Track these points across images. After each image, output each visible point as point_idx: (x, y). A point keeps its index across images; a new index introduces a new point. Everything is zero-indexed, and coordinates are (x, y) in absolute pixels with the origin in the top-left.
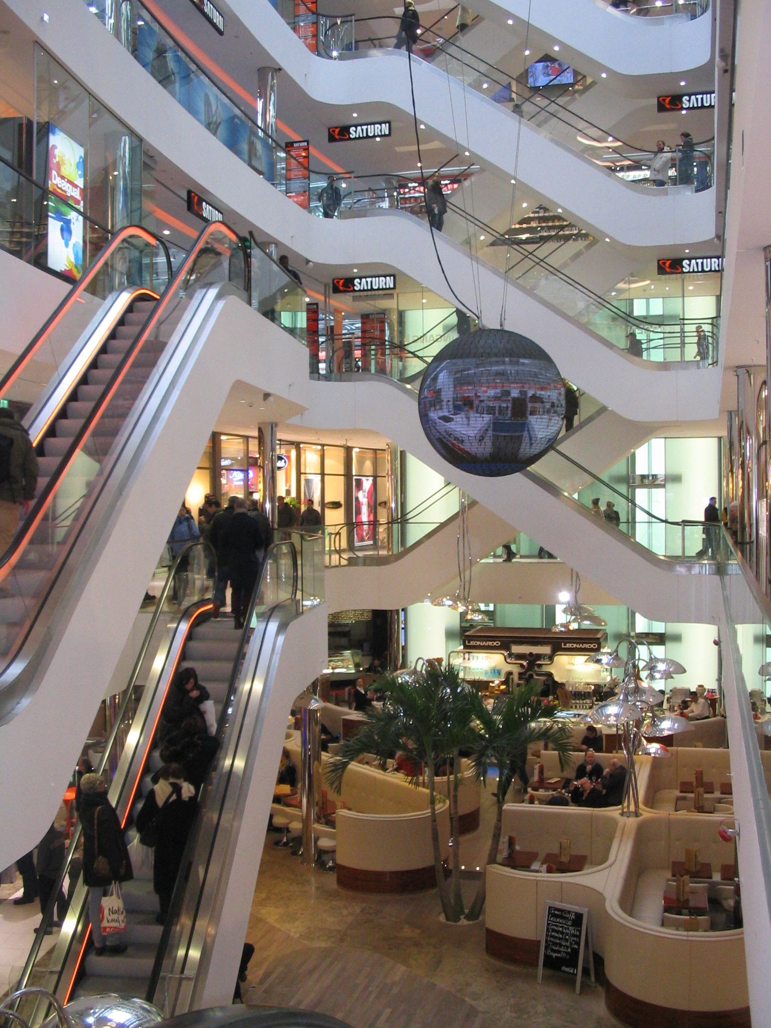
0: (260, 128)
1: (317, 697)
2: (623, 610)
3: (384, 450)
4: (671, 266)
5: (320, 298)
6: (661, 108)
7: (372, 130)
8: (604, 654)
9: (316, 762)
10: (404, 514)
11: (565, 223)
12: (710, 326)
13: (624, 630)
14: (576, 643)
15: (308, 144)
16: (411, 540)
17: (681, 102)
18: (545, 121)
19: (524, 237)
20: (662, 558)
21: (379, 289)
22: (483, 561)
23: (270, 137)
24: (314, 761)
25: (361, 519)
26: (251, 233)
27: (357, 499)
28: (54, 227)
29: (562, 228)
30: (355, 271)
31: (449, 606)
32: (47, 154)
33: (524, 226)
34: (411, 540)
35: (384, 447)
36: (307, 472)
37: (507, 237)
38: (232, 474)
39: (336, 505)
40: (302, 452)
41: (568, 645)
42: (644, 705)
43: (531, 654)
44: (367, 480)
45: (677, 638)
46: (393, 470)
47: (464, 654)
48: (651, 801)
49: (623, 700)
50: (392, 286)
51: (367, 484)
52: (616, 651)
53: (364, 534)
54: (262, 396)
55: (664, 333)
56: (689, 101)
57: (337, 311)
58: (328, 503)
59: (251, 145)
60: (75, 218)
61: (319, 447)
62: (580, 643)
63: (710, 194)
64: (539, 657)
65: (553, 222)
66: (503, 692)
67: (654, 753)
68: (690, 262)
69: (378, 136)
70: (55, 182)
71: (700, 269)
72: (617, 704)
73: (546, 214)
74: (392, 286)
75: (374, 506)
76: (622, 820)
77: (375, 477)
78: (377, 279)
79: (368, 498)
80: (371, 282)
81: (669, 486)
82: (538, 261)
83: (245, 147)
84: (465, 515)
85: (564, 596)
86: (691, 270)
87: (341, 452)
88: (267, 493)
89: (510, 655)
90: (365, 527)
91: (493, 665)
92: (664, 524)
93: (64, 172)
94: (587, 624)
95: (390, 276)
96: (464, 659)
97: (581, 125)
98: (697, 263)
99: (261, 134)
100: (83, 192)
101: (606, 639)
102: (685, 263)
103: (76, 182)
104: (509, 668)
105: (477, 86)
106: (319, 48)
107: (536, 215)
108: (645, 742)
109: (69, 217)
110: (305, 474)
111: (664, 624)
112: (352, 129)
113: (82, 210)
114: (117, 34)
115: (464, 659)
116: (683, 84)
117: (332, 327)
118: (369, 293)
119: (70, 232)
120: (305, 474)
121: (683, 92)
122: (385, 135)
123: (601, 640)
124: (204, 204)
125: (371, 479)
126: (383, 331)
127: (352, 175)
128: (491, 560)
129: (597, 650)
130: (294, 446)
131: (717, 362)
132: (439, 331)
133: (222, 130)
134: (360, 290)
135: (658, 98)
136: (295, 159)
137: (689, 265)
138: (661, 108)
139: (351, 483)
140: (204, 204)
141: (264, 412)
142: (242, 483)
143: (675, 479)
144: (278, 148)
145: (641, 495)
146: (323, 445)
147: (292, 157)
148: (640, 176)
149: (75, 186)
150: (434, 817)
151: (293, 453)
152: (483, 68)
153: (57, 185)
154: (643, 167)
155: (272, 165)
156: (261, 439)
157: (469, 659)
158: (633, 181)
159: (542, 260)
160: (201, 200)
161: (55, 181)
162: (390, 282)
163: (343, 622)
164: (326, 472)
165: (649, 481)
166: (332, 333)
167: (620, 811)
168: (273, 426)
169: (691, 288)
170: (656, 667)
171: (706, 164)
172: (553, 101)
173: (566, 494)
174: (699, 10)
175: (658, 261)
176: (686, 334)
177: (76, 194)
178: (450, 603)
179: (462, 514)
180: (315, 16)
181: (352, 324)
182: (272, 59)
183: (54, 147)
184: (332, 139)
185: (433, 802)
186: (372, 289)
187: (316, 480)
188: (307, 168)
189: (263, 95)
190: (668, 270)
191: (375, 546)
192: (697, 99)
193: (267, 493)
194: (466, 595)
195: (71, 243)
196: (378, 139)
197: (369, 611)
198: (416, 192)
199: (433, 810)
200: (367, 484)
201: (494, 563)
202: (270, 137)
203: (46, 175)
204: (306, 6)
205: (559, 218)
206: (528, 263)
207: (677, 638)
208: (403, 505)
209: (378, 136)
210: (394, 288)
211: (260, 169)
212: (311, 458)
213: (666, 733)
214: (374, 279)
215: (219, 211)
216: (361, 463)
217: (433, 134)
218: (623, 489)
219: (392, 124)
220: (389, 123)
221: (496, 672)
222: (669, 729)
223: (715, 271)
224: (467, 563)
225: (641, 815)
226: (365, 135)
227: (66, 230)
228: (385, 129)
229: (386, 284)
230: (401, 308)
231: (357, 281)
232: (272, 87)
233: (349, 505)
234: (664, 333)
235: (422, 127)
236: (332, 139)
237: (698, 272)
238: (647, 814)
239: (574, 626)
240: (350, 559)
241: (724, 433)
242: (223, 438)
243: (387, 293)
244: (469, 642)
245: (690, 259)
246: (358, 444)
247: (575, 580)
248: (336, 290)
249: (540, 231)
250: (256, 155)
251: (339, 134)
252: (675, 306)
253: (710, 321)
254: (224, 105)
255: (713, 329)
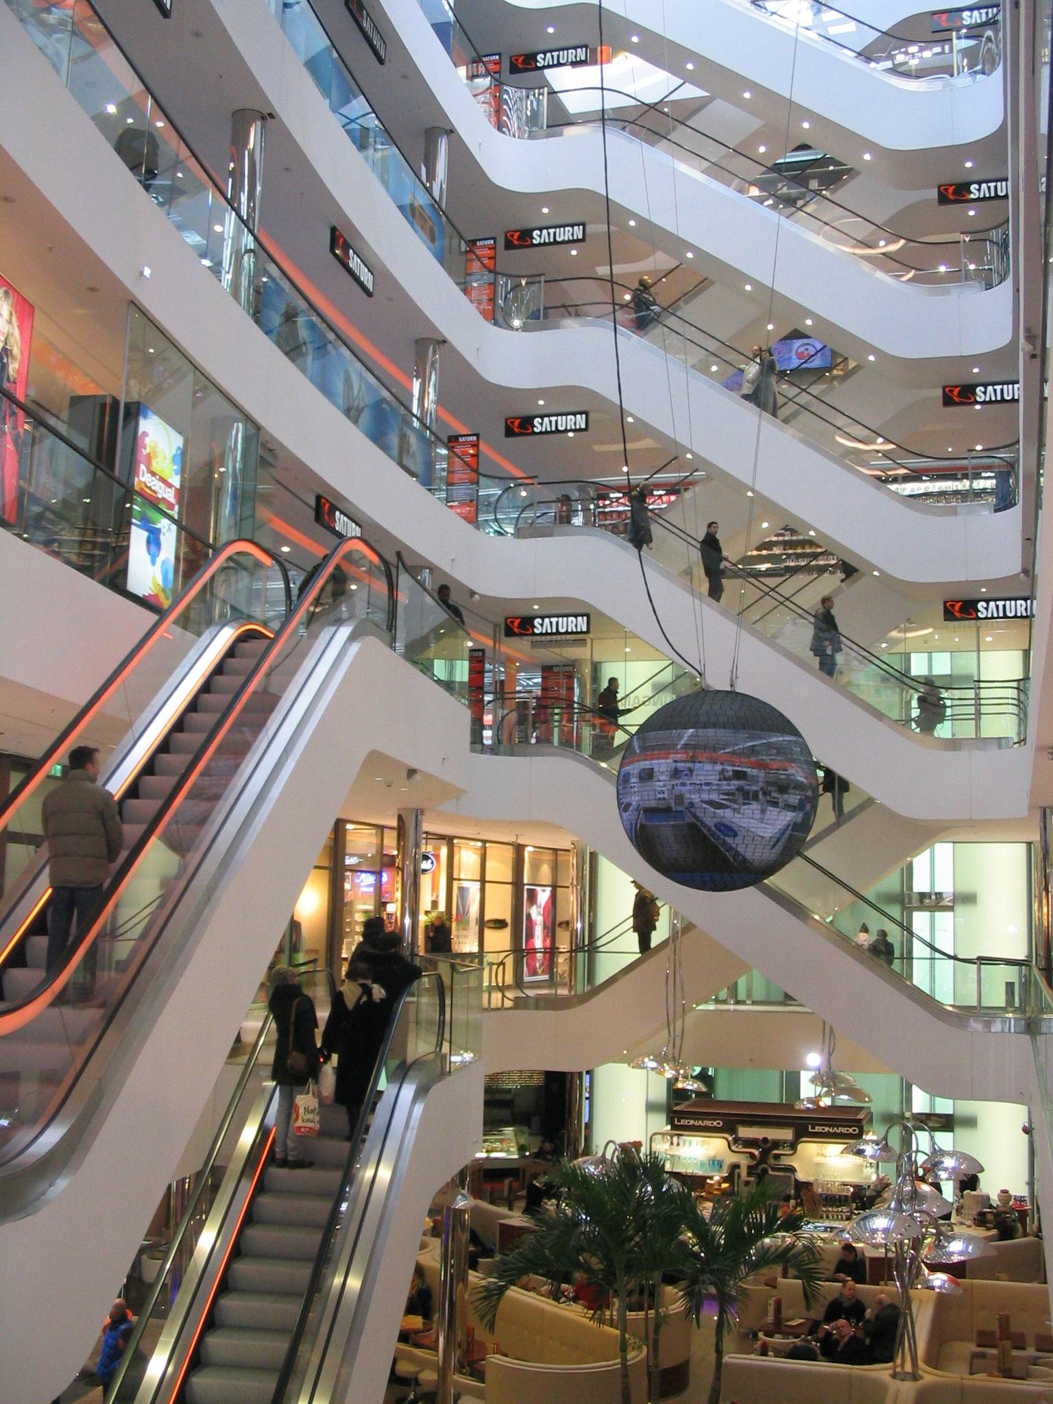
0: (416, 417)
1: (465, 1192)
2: (894, 1081)
3: (568, 851)
4: (962, 610)
5: (488, 643)
6: (948, 401)
7: (564, 422)
8: (867, 1142)
9: (461, 1285)
10: (593, 940)
11: (819, 550)
12: (1016, 691)
13: (896, 1109)
14: (829, 1126)
15: (478, 439)
16: (602, 975)
17: (974, 393)
18: (794, 415)
19: (763, 567)
20: (950, 1009)
21: (567, 633)
22: (700, 1007)
23: (428, 428)
24: (458, 1283)
25: (533, 944)
26: (399, 554)
27: (529, 916)
28: (138, 537)
29: (815, 556)
30: (536, 607)
31: (653, 1069)
32: (134, 441)
33: (764, 552)
34: (602, 975)
35: (568, 846)
36: (462, 877)
37: (741, 566)
38: (358, 877)
39: (500, 924)
40: (456, 849)
41: (817, 1129)
42: (925, 1217)
43: (765, 1140)
44: (544, 891)
45: (970, 1122)
46: (581, 878)
47: (672, 1137)
48: (935, 1358)
49: (895, 1210)
50: (584, 629)
51: (543, 896)
52: (885, 1138)
53: (538, 965)
54: (405, 774)
55: (952, 699)
56: (985, 393)
57: (509, 661)
58: (489, 921)
59: (403, 438)
60: (167, 527)
61: (479, 844)
62: (834, 1126)
63: (1015, 514)
64: (777, 1144)
65: (803, 548)
66: (724, 1192)
67: (940, 1287)
68: (988, 604)
69: (571, 430)
70: (143, 479)
71: (1001, 614)
72: (887, 1215)
73: (794, 538)
74: (584, 629)
75: (552, 927)
76: (894, 1384)
77: (554, 887)
78: (565, 619)
79: (543, 915)
80: (557, 623)
81: (959, 909)
82: (782, 599)
83: (394, 440)
84: (677, 943)
85: (814, 1059)
86: (989, 616)
87: (509, 852)
88: (407, 905)
89: (736, 1140)
90: (539, 956)
91: (712, 1153)
92: (952, 961)
93: (156, 466)
94: (844, 1099)
95: (582, 615)
96: (672, 1144)
97: (841, 421)
98: (997, 607)
99: (416, 424)
100: (179, 493)
101: (871, 1121)
102: (981, 605)
103: (170, 481)
104: (735, 1159)
105: (703, 368)
106: (496, 315)
107: (781, 538)
108: (926, 1271)
109: (158, 526)
110: (459, 880)
111: (951, 1101)
112: (537, 421)
113: (176, 517)
114: (236, 294)
115: (672, 1144)
116: (976, 370)
117: (502, 682)
118: (554, 638)
119: (158, 545)
120: (459, 880)
121: (975, 381)
122: (580, 430)
123: (864, 1123)
124: (337, 513)
125: (549, 889)
126: (571, 689)
127: (535, 481)
128: (712, 1007)
129: (859, 1136)
130: (444, 842)
131: (1024, 740)
132: (647, 691)
133: (365, 418)
134: (541, 634)
135: (944, 388)
136: (459, 457)
137: (987, 609)
138: (948, 401)
139: (521, 894)
140: (337, 513)
141: (408, 795)
142: (372, 889)
143: (968, 899)
144: (438, 443)
145: (920, 920)
146: (484, 842)
147: (457, 455)
148: (919, 489)
149: (169, 485)
150: (625, 1369)
151: (444, 851)
152: (712, 345)
153: (145, 483)
154: (924, 478)
155: (429, 464)
156: (401, 830)
157: (678, 1144)
158: (910, 496)
159: (788, 599)
160: (334, 508)
161: (143, 478)
162: (582, 623)
163: (505, 1087)
164: (487, 879)
165: (933, 902)
166: (502, 691)
167: (891, 1372)
168: (419, 813)
169: (989, 639)
170: (942, 1162)
171: (1008, 474)
172: (804, 390)
173: (817, 917)
174: (995, 281)
175: (945, 603)
176: (982, 702)
177: (170, 496)
178: (654, 1064)
179: (673, 941)
180: (492, 275)
181: (529, 679)
182: (436, 329)
183: (145, 434)
184: (509, 432)
185: (624, 1348)
186: (558, 633)
187: (474, 888)
188: (476, 471)
189: (421, 374)
190: (958, 615)
191: (552, 983)
192: (995, 391)
193: (407, 905)
194: (677, 1055)
195: (159, 560)
196: (571, 434)
197: (541, 1073)
198: (619, 504)
199: (624, 1359)
200: (543, 896)
201: (735, 1010)
202: (428, 428)
203: (132, 469)
204: (481, 262)
205: (810, 543)
206: (768, 603)
207: (970, 1122)
208: (592, 927)
209: (571, 430)
210: (588, 632)
211: (413, 468)
212: (468, 858)
213: (956, 1259)
214: (560, 619)
215: (357, 524)
216: (536, 867)
217: (645, 429)
218: (895, 911)
219: (591, 416)
220: (586, 413)
221: (716, 1163)
222: (960, 1253)
223: (1022, 617)
224: (679, 1010)
225: (922, 1378)
226: (554, 429)
227: (154, 541)
228: (581, 421)
229: (576, 626)
230: (596, 659)
231: (537, 621)
232: (433, 364)
233: (518, 924)
234: (952, 699)
235: (630, 420)
236: (509, 432)
237: (998, 618)
238: (929, 1376)
239: (826, 1102)
240: (516, 1000)
241: (1036, 837)
242: (349, 826)
243: (578, 638)
244: (679, 1121)
245: (987, 601)
246: (532, 842)
247: (828, 1037)
248: (509, 632)
249: (785, 560)
250: (408, 451)
251: (520, 426)
252: (967, 663)
253: (1015, 684)
254: (369, 386)
255: (1019, 695)
